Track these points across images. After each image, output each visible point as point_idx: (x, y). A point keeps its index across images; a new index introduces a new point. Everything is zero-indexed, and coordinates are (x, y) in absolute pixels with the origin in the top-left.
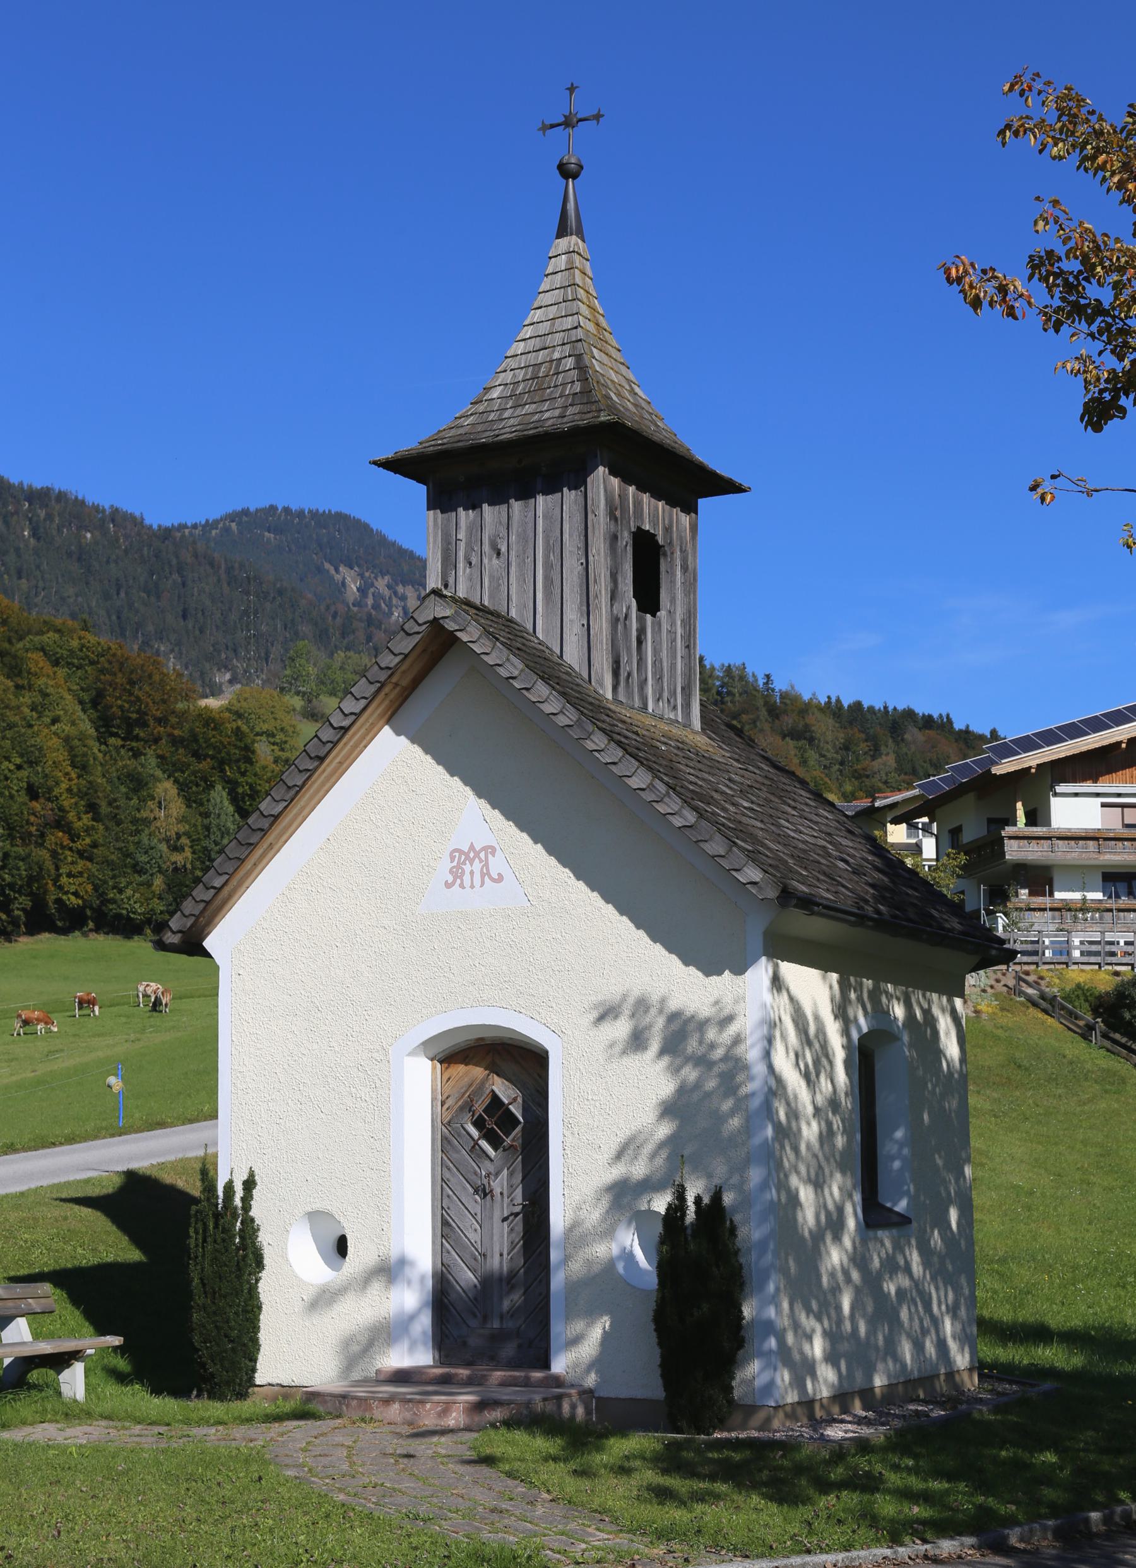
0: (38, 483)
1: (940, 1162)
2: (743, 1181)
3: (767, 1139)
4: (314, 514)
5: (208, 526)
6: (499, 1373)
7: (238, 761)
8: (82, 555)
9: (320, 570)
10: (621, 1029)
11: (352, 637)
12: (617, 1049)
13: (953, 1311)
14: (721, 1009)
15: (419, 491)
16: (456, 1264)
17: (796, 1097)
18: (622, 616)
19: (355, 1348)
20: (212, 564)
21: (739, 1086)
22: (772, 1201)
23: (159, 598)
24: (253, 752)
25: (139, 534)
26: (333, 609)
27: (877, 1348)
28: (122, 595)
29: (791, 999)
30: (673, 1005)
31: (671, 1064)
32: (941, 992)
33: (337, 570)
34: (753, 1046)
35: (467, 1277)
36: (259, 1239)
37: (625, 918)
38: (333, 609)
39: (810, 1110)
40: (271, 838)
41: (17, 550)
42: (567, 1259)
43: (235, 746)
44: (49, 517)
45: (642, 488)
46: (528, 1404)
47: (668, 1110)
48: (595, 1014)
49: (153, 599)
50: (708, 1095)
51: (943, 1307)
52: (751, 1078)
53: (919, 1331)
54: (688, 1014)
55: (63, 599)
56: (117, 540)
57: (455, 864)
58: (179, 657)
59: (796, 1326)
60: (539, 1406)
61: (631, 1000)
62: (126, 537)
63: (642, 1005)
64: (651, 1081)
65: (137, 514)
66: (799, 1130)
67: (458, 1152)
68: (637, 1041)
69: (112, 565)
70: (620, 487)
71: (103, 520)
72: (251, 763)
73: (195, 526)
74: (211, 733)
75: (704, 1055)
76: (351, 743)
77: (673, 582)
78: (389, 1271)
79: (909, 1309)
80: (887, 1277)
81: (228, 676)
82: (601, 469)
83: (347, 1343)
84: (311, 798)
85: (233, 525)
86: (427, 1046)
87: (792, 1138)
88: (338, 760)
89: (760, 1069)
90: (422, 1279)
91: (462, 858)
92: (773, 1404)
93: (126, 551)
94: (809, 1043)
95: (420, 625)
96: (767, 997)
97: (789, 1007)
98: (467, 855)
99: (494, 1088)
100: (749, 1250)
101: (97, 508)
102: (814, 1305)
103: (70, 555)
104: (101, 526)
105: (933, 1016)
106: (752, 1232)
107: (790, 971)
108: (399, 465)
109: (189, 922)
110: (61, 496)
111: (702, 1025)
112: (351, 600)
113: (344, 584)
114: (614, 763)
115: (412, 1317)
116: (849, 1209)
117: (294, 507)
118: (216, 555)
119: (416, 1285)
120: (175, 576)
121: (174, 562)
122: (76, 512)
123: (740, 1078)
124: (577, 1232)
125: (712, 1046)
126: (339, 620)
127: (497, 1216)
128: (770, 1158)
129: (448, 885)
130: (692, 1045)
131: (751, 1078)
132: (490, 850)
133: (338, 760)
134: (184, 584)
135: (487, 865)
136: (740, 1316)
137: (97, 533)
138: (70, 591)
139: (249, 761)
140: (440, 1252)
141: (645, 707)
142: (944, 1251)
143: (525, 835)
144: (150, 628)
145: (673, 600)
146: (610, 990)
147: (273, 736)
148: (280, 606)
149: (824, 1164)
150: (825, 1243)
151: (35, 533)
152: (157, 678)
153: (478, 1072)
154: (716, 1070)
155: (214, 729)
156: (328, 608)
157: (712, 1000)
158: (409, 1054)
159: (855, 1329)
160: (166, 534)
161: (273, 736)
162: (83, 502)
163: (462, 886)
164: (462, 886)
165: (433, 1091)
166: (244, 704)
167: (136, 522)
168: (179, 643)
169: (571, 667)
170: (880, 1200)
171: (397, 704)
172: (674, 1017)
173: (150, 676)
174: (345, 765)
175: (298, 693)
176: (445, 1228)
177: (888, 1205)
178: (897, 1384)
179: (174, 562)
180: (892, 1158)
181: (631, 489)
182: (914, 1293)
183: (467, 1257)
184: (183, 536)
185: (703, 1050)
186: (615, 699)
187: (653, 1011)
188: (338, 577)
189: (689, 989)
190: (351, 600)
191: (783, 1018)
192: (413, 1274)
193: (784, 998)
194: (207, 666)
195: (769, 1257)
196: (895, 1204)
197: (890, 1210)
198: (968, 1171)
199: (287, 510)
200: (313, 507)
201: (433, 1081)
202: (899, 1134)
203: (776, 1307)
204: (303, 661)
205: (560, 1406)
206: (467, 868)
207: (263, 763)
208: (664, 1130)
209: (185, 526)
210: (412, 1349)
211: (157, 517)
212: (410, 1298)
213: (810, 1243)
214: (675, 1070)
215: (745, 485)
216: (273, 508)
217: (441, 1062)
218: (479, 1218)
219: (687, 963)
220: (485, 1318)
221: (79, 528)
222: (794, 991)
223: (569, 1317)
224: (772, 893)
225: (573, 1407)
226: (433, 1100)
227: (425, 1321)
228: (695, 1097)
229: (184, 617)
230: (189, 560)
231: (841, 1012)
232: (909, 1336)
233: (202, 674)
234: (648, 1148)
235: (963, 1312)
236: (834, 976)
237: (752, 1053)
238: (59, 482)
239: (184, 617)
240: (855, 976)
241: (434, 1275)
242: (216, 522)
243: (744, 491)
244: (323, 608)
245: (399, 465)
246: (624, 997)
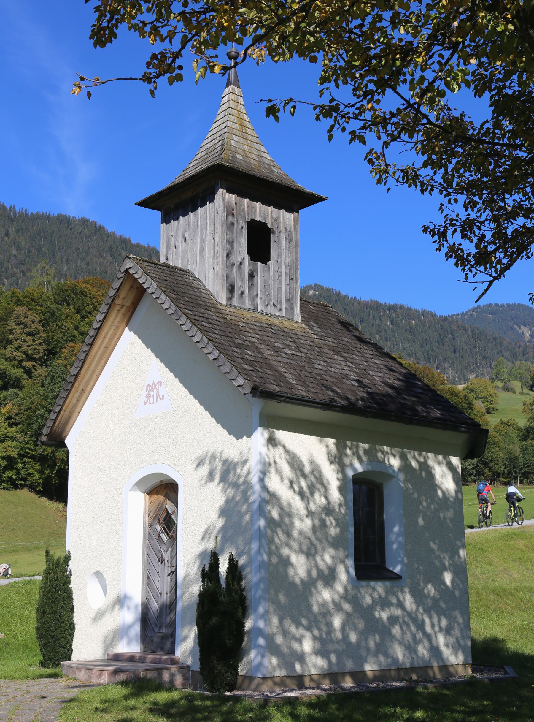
0: (392, 302)
1: (435, 547)
2: (250, 549)
3: (259, 527)
4: (508, 305)
5: (464, 314)
6: (150, 656)
7: (466, 409)
8: (411, 330)
9: (512, 328)
10: (205, 470)
11: (527, 356)
12: (204, 480)
13: (448, 632)
14: (242, 457)
15: (158, 214)
16: (151, 599)
17: (290, 505)
18: (237, 264)
19: (108, 642)
20: (465, 330)
21: (248, 498)
22: (263, 561)
23: (443, 345)
24: (473, 405)
25: (434, 320)
26: (518, 344)
27: (368, 649)
28: (429, 345)
29: (287, 451)
30: (225, 456)
31: (224, 487)
32: (436, 453)
33: (520, 328)
34: (254, 475)
35: (155, 606)
36: (70, 586)
37: (207, 412)
38: (518, 344)
39: (304, 512)
40: (79, 384)
41: (385, 330)
42: (183, 594)
43: (465, 403)
44: (397, 316)
45: (252, 199)
46: (135, 672)
47: (224, 512)
48: (195, 464)
49: (441, 346)
50: (237, 503)
51: (437, 628)
52: (254, 493)
53: (411, 641)
54: (230, 460)
55: (404, 349)
56: (425, 323)
58: (453, 369)
59: (285, 633)
60: (142, 674)
61: (209, 455)
62: (429, 321)
63: (213, 456)
64: (215, 496)
65: (433, 311)
66: (292, 524)
67: (153, 540)
68: (211, 476)
69: (424, 333)
70: (236, 199)
71: (419, 315)
72: (472, 410)
73: (458, 315)
74: (454, 398)
75: (235, 483)
76: (109, 336)
77: (280, 247)
78: (121, 601)
79: (402, 628)
80: (378, 608)
81: (474, 376)
82: (221, 190)
83: (106, 638)
84: (96, 366)
85: (474, 313)
86: (139, 484)
87: (284, 528)
88: (104, 345)
89: (257, 487)
90: (136, 606)
91: (151, 388)
92: (260, 676)
93: (429, 327)
94: (304, 476)
96: (264, 450)
97: (284, 456)
98: (152, 387)
99: (167, 506)
100: (251, 588)
101: (416, 311)
102: (304, 622)
103: (406, 330)
104: (419, 317)
105: (428, 466)
106: (252, 578)
107: (281, 435)
108: (146, 203)
109: (49, 430)
110: (401, 307)
111: (235, 465)
112: (527, 340)
113: (523, 333)
114: (188, 330)
115: (130, 627)
116: (341, 569)
117: (500, 303)
118: (466, 325)
119: (133, 610)
120: (450, 336)
121: (449, 330)
122: (408, 313)
123: (249, 493)
124: (188, 579)
125: (239, 477)
126: (521, 349)
127: (166, 574)
128: (266, 539)
129: (145, 403)
130: (231, 477)
131: (254, 493)
132: (160, 383)
133: (104, 345)
134: (454, 339)
135: (158, 392)
136: (242, 625)
137: (417, 321)
138: (407, 345)
139: (471, 409)
140: (145, 592)
141: (256, 309)
142: (437, 596)
143: (172, 374)
144: (441, 358)
145: (280, 255)
146: (201, 450)
147: (487, 398)
148: (495, 345)
149: (315, 542)
150: (316, 587)
151: (392, 323)
152: (430, 376)
153: (161, 498)
154: (240, 490)
155: (455, 396)
156: (516, 344)
157: (239, 452)
158: (131, 490)
159: (345, 637)
160: (445, 319)
161: (487, 398)
162: (410, 309)
163: (150, 403)
164: (150, 403)
165: (145, 509)
166: (473, 386)
167: (433, 315)
168: (453, 363)
169: (208, 290)
170: (387, 566)
171: (128, 316)
172: (226, 461)
173: (427, 376)
174: (110, 349)
175: (500, 380)
176: (148, 581)
177: (391, 569)
178: (390, 670)
179: (449, 330)
180: (393, 543)
181: (246, 201)
182: (406, 619)
183: (155, 595)
184: (453, 319)
185: (235, 480)
186: (230, 305)
187: (217, 460)
188: (520, 331)
189: (230, 446)
190: (527, 340)
191: (278, 460)
192: (132, 604)
193: (280, 450)
194: (465, 372)
195: (259, 592)
196: (394, 569)
197: (392, 572)
198: (462, 552)
199: (496, 305)
200: (508, 303)
201: (145, 503)
202: (396, 529)
203: (265, 621)
204: (501, 367)
205: (160, 675)
206: (152, 394)
207: (477, 409)
208: (220, 523)
209: (454, 315)
210: (129, 643)
211: (441, 312)
212: (130, 616)
213: (300, 587)
214: (225, 490)
215: (323, 195)
216: (490, 304)
217: (148, 494)
218: (160, 574)
219: (230, 434)
220: (160, 627)
221: (409, 319)
222: (289, 446)
223: (182, 627)
224: (248, 390)
225: (172, 676)
226: (145, 513)
227: (137, 628)
228: (233, 504)
229: (455, 352)
230: (455, 329)
231: (337, 460)
232: (401, 643)
233: (463, 375)
234: (214, 533)
235: (457, 632)
236: (331, 442)
237: (254, 479)
238: (400, 301)
239: (455, 352)
240: (351, 440)
241: (143, 604)
242: (467, 312)
243: (323, 199)
244: (514, 344)
245: (146, 203)
246: (207, 453)
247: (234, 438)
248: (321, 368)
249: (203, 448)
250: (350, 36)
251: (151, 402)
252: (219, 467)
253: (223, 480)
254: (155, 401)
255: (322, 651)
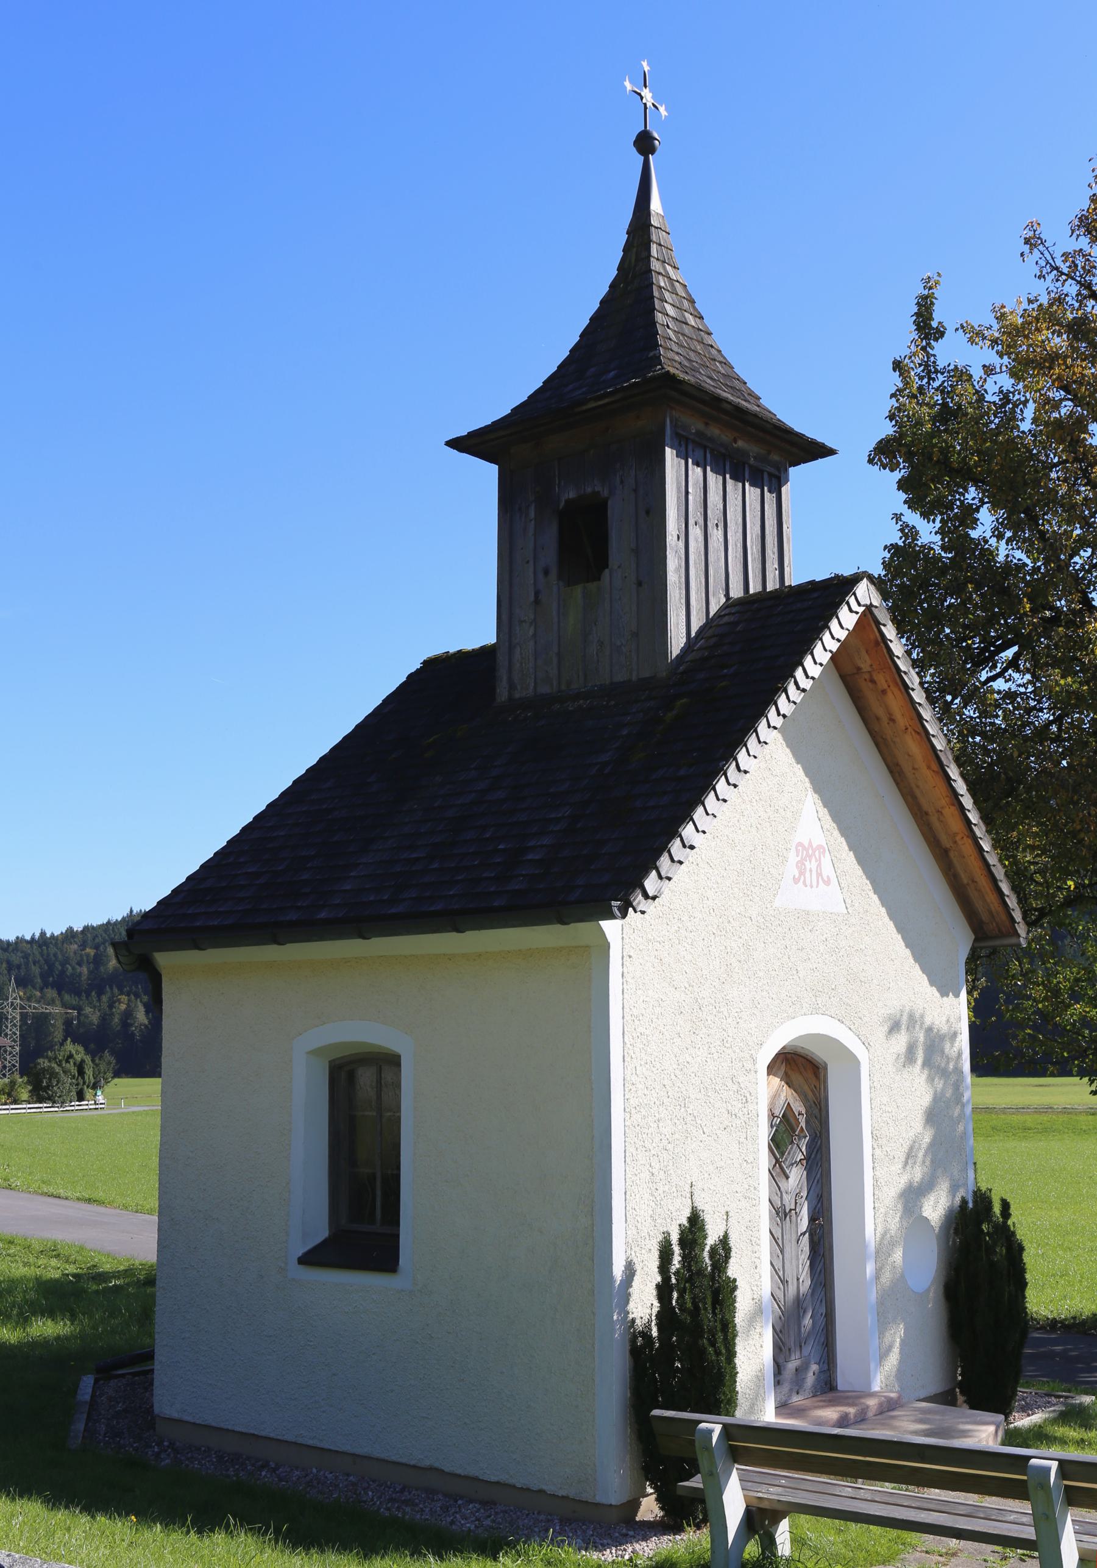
10: (900, 1042)
30: (928, 1021)
57: (799, 858)
68: (910, 1056)
91: (807, 852)
95: (859, 604)
111: (942, 1038)
129: (796, 881)
206: (807, 863)
214: (930, 1080)
247: (937, 994)
248: (571, 387)
249: (895, 1002)
250: (1051, 723)
251: (808, 882)
252: (922, 1039)
253: (927, 1063)
254: (814, 883)
255: (1035, 421)
